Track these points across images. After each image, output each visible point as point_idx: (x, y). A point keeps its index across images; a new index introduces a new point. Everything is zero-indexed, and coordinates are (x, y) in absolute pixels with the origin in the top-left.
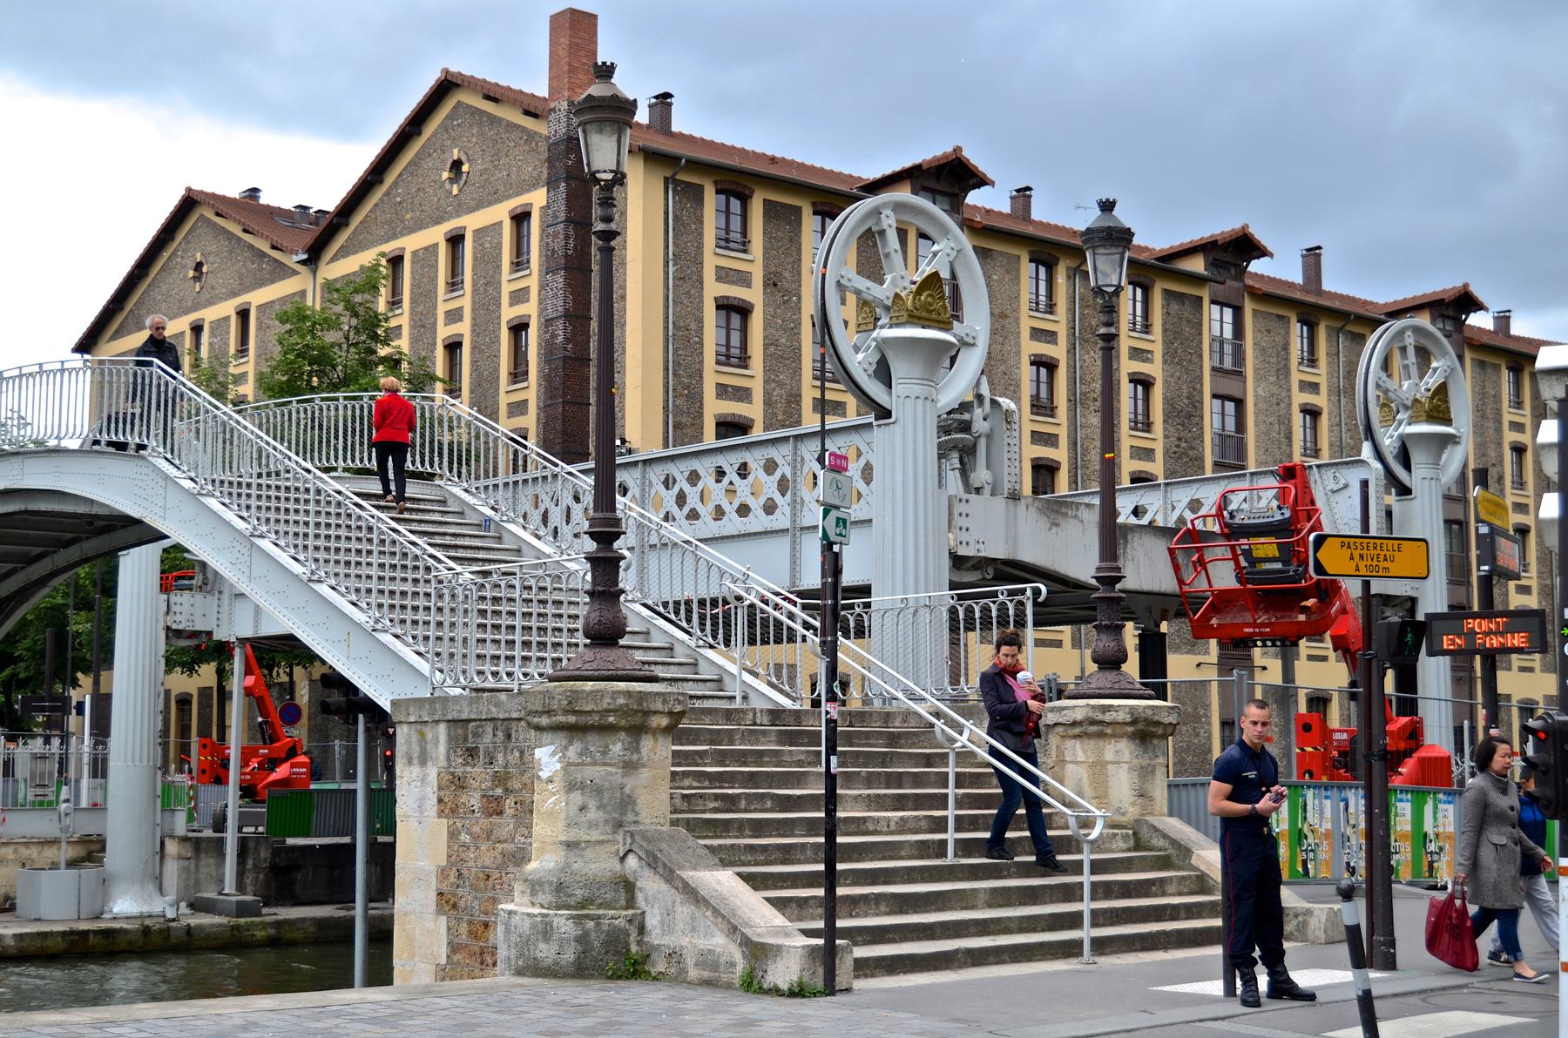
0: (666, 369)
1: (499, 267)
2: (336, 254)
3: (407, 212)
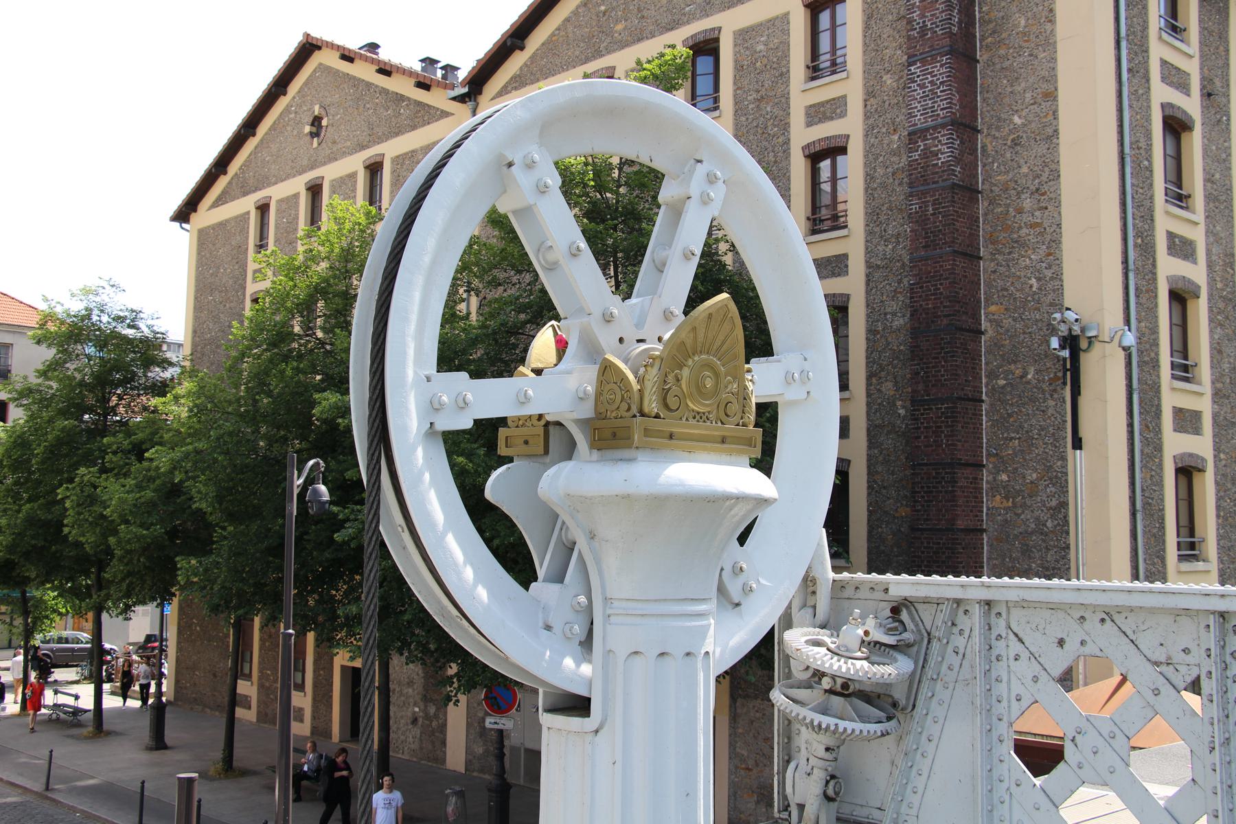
2: (505, 87)
3: (617, 21)
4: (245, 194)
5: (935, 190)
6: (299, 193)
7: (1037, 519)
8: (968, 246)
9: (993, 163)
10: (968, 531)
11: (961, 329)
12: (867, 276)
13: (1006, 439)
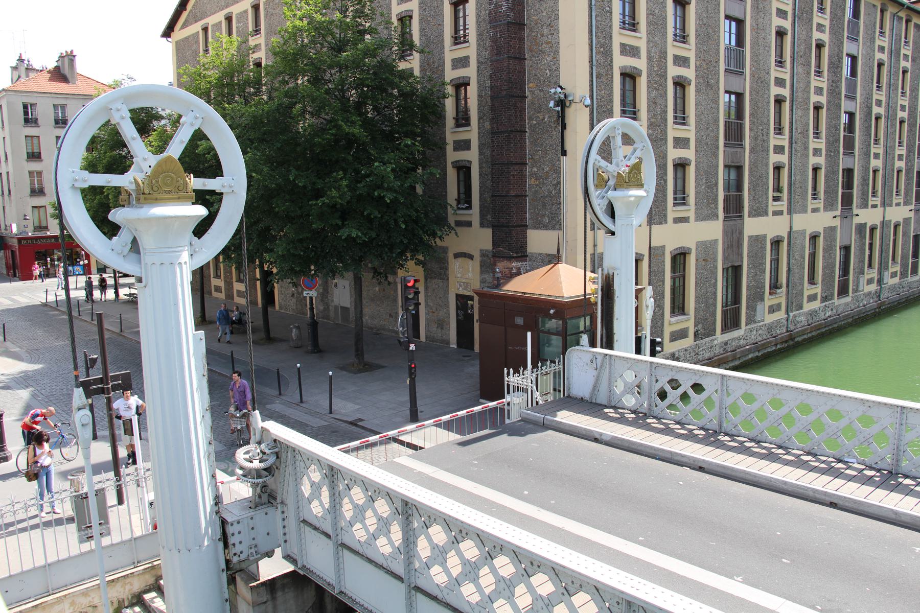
0: (591, 31)
4: (196, 22)
5: (500, 25)
7: (548, 190)
8: (518, 53)
9: (531, 9)
10: (517, 196)
11: (513, 96)
12: (478, 67)
13: (535, 150)
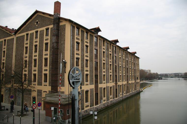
1: (44, 36)
6: (86, 108)
